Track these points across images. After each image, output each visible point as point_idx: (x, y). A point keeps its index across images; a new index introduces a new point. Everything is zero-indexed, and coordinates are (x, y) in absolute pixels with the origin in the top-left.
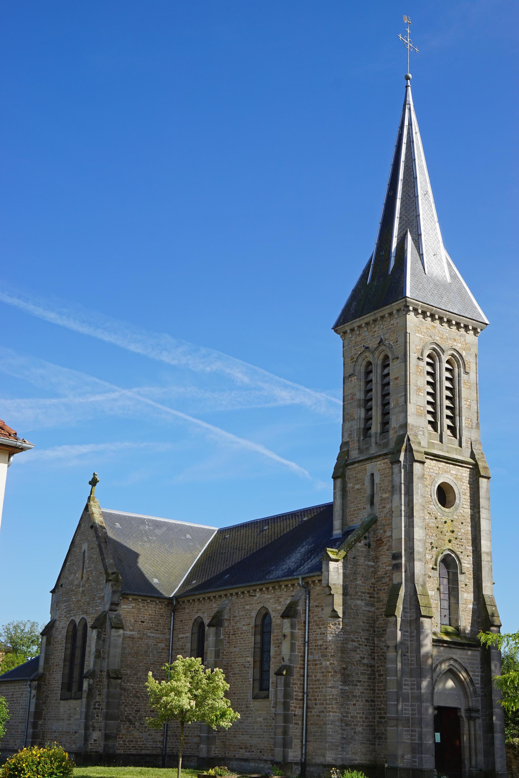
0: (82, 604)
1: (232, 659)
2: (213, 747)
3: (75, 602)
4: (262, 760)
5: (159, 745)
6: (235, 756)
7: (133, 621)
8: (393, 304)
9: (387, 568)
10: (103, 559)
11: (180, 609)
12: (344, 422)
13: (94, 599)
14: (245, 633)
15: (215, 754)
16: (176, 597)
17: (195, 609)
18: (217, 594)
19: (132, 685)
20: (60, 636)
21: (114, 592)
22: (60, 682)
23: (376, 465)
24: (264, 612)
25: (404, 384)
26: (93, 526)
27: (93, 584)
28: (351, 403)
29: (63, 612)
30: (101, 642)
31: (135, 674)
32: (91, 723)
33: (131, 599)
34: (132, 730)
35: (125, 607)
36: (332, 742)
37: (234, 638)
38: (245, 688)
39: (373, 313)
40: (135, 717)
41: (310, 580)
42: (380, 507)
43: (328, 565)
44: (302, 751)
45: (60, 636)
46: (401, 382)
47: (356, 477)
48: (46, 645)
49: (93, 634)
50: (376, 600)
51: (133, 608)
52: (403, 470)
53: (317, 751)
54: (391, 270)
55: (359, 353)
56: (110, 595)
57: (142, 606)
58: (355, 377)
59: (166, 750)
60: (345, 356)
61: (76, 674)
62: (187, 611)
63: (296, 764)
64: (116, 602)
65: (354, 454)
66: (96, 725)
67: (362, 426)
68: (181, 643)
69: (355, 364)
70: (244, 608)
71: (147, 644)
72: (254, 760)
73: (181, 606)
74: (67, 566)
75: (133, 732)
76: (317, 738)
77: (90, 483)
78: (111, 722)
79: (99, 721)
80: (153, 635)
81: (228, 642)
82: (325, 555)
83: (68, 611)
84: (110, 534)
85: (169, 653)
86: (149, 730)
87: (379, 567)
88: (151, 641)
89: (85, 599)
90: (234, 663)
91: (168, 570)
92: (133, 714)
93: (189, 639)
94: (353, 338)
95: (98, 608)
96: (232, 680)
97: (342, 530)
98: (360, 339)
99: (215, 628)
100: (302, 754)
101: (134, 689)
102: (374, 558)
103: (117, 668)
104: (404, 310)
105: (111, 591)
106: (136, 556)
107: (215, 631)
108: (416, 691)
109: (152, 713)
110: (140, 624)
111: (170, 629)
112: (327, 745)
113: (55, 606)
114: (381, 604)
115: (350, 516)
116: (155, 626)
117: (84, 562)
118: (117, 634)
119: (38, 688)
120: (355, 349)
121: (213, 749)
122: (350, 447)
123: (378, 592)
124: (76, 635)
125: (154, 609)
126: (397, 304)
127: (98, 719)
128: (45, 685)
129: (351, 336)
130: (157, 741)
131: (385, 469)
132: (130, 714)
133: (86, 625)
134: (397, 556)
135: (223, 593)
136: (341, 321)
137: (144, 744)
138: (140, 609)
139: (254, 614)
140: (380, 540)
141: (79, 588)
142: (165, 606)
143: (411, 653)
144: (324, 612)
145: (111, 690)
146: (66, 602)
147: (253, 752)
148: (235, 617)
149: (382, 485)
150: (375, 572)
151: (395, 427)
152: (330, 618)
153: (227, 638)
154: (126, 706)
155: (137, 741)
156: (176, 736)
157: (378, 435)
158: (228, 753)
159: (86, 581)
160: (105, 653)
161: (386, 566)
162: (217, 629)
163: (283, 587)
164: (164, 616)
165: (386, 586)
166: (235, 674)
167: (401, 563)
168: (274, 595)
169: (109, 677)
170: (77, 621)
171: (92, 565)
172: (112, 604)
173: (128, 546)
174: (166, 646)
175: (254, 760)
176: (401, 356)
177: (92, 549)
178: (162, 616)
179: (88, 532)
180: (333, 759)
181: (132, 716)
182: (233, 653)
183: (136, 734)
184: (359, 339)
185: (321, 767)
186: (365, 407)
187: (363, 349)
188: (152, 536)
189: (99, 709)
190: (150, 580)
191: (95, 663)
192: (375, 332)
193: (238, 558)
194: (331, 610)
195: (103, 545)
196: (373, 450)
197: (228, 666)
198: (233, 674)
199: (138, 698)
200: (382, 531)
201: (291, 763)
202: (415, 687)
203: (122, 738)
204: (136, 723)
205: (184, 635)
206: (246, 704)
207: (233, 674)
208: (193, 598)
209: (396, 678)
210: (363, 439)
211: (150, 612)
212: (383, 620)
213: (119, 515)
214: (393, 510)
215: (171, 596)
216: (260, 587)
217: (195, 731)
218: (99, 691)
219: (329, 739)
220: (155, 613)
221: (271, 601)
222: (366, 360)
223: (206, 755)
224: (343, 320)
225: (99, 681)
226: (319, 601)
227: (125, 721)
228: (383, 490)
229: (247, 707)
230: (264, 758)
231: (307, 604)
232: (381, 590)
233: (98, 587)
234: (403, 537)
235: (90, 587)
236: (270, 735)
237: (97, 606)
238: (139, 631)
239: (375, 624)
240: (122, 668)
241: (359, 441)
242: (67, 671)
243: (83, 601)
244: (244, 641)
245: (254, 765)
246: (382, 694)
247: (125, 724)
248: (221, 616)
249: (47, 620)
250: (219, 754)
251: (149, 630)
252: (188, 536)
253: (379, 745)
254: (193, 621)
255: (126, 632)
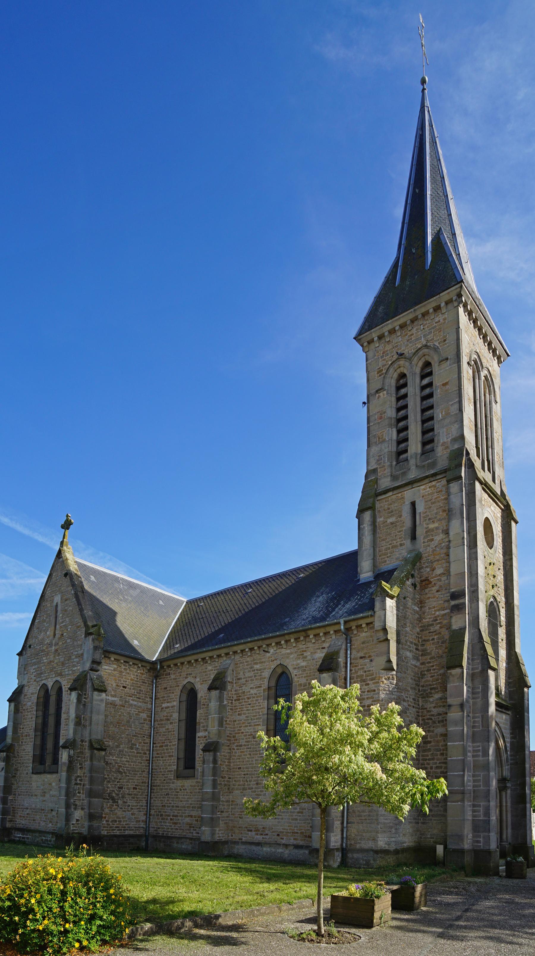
0: (55, 665)
1: (236, 729)
2: (217, 829)
3: (46, 664)
4: (280, 844)
5: (142, 825)
6: (242, 839)
7: (114, 685)
8: (441, 294)
9: (437, 613)
10: (81, 610)
11: (163, 675)
12: (369, 446)
13: (70, 658)
14: (254, 697)
15: (219, 837)
16: (160, 661)
17: (184, 674)
18: (215, 654)
19: (114, 758)
20: (29, 704)
21: (96, 648)
22: (31, 754)
23: (419, 490)
24: (279, 671)
25: (457, 388)
26: (68, 574)
27: (69, 641)
28: (379, 423)
29: (32, 676)
30: (82, 707)
31: (118, 746)
32: (72, 801)
33: (112, 659)
34: (115, 809)
35: (107, 667)
36: (384, 823)
37: (238, 704)
38: (254, 762)
39: (412, 310)
40: (118, 795)
41: (353, 625)
42: (426, 540)
43: (384, 602)
44: (342, 834)
45: (29, 704)
46: (452, 387)
47: (389, 509)
48: (14, 712)
49: (70, 700)
50: (420, 653)
51: (114, 670)
52: (464, 489)
53: (364, 834)
54: (429, 264)
55: (390, 363)
56: (91, 652)
57: (124, 669)
58: (385, 392)
59: (149, 830)
60: (369, 370)
61: (50, 745)
62: (173, 676)
63: (337, 849)
64: (98, 660)
65: (385, 483)
66: (77, 803)
67: (394, 449)
68: (165, 714)
69: (384, 377)
70: (251, 668)
71: (129, 713)
72: (270, 844)
73: (165, 671)
74: (36, 624)
75: (116, 811)
76: (363, 818)
77: (63, 527)
78: (95, 800)
79: (81, 798)
80: (135, 703)
81: (231, 709)
82: (379, 589)
83: (38, 674)
84: (86, 587)
85: (151, 725)
86: (132, 809)
87: (424, 613)
88: (133, 709)
89: (59, 659)
90: (239, 733)
91: (149, 632)
92: (116, 792)
93: (176, 709)
94: (380, 348)
95: (75, 668)
96: (236, 753)
97: (374, 573)
98: (391, 347)
99: (218, 691)
100: (342, 838)
101: (116, 763)
102: (419, 603)
103: (99, 737)
104: (456, 300)
105: (92, 647)
106: (114, 614)
107: (218, 695)
108: (481, 758)
109: (135, 790)
110: (122, 690)
111: (152, 698)
112: (379, 827)
113: (22, 670)
114: (429, 657)
115: (380, 556)
116: (137, 693)
117: (56, 617)
118: (100, 698)
119: (7, 760)
120: (384, 360)
121: (217, 832)
122: (379, 474)
123: (424, 643)
124: (49, 703)
125: (136, 674)
126: (448, 293)
127: (80, 797)
128: (15, 757)
129: (378, 345)
130: (140, 821)
131: (432, 494)
132: (113, 791)
133: (60, 689)
134: (458, 595)
135: (223, 652)
136: (366, 327)
137: (128, 824)
138: (121, 672)
139: (266, 674)
140: (427, 579)
141: (51, 647)
142: (147, 671)
143: (473, 713)
144: (373, 663)
145: (94, 763)
146: (35, 665)
147: (267, 834)
148: (239, 679)
149: (428, 513)
150: (420, 619)
151: (445, 443)
152: (383, 671)
153: (230, 704)
154: (109, 782)
155: (120, 821)
156: (162, 815)
157: (419, 456)
158: (232, 836)
159: (59, 639)
160: (86, 720)
161: (435, 611)
162: (220, 692)
163: (311, 637)
164: (146, 683)
165: (436, 634)
166: (241, 746)
167: (465, 603)
168: (296, 649)
169: (91, 747)
170: (50, 685)
171: (67, 619)
172: (94, 662)
173: (105, 602)
174: (148, 716)
175: (270, 844)
176: (451, 355)
177: (66, 600)
178: (144, 683)
179: (61, 582)
180: (386, 844)
181: (115, 793)
182: (237, 722)
183: (119, 813)
184: (388, 347)
185: (372, 853)
186: (397, 428)
187: (396, 356)
188: (127, 596)
189: (80, 784)
190: (131, 642)
191: (75, 732)
192: (412, 334)
193: (226, 619)
194: (386, 660)
195: (80, 594)
196: (413, 474)
197: (231, 737)
198: (237, 746)
199: (121, 773)
200: (428, 570)
201: (333, 849)
202: (480, 753)
203: (105, 818)
204: (119, 801)
205: (169, 705)
206: (257, 780)
207: (237, 746)
208: (182, 660)
209: (462, 743)
210: (396, 465)
211: (132, 676)
212: (432, 677)
213: (93, 568)
214: (451, 539)
215: (154, 660)
216: (277, 640)
217: (186, 810)
218: (81, 764)
219: (382, 819)
220: (137, 679)
221: (291, 656)
222: (399, 371)
223: (209, 838)
224: (369, 326)
225: (80, 752)
226: (365, 651)
227: (107, 799)
228: (429, 519)
229: (257, 784)
230: (283, 842)
231: (349, 656)
232: (428, 640)
233: (75, 643)
234: (466, 571)
235: (65, 645)
236: (292, 816)
237: (74, 666)
238: (121, 697)
239: (419, 682)
240: (104, 738)
241: (391, 466)
242: (38, 742)
243: (56, 661)
244: (253, 707)
245: (269, 849)
246: (428, 764)
247: (109, 802)
248: (224, 677)
249: (15, 686)
250: (223, 837)
251: (131, 697)
252: (161, 602)
253: (423, 823)
254: (181, 688)
255: (108, 698)
